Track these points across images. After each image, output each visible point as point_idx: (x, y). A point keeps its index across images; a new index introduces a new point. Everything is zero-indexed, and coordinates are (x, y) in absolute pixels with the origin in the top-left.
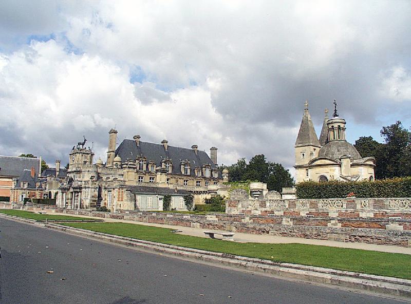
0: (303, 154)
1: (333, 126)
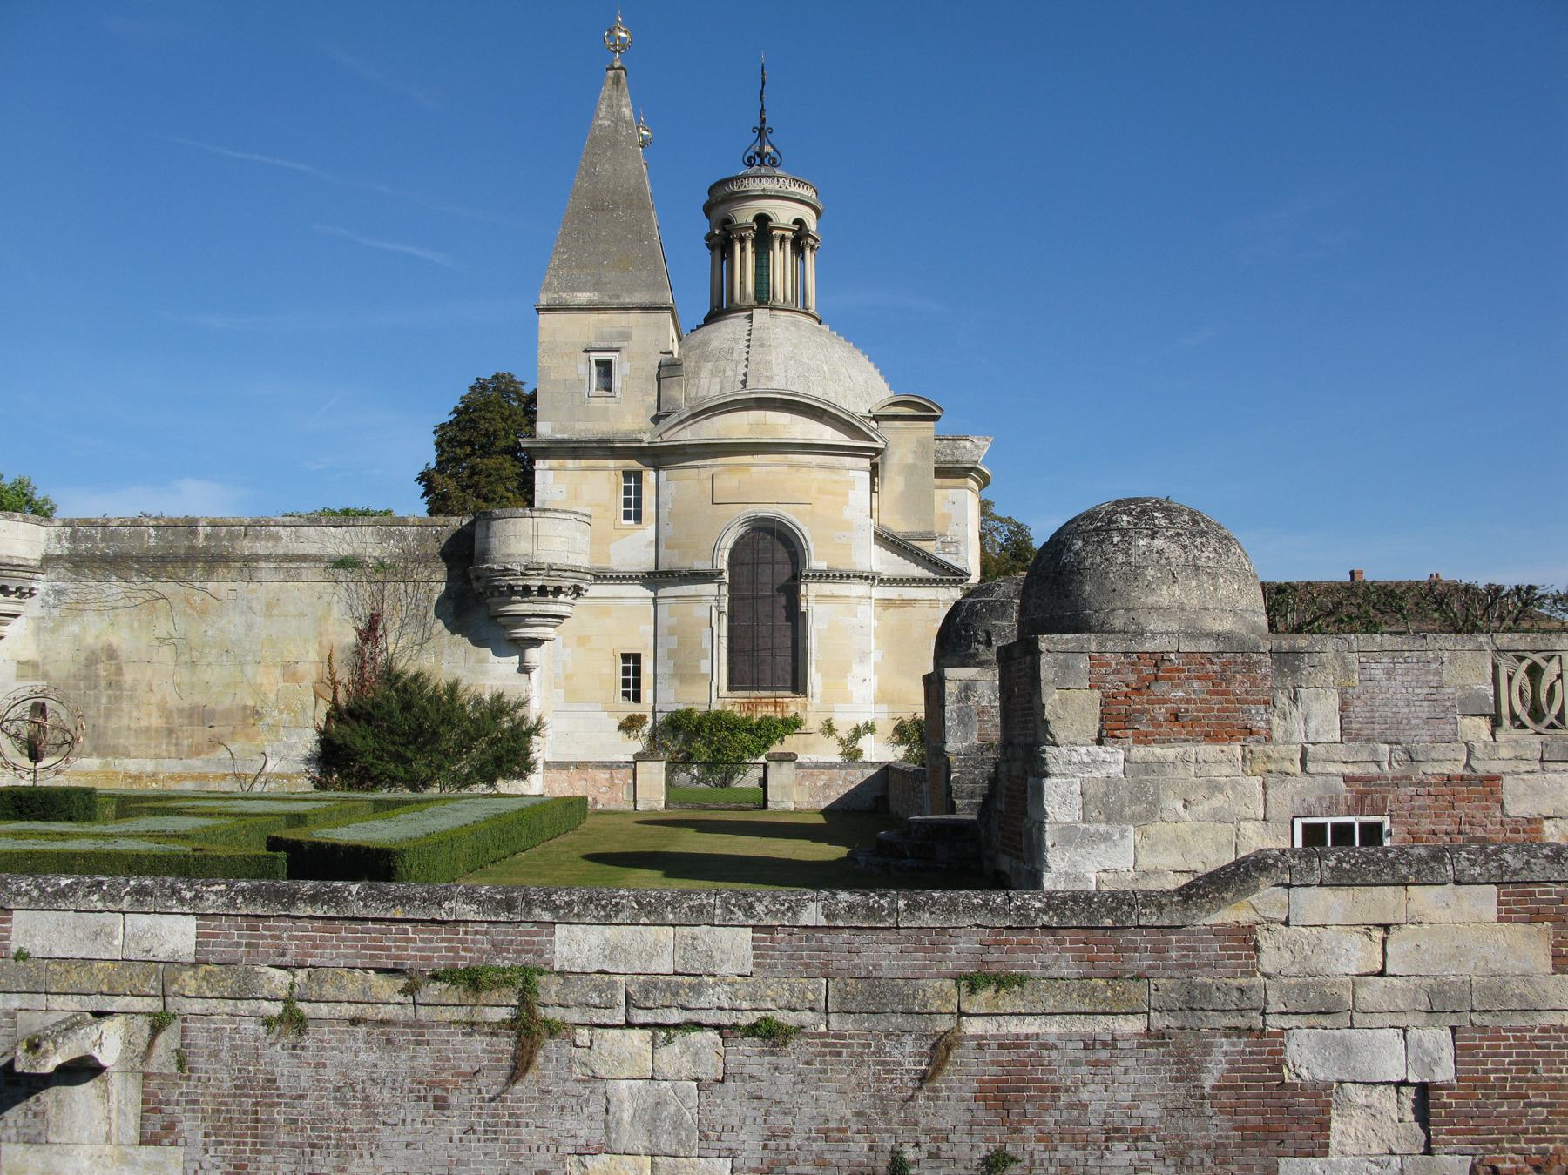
0: (605, 368)
1: (763, 219)
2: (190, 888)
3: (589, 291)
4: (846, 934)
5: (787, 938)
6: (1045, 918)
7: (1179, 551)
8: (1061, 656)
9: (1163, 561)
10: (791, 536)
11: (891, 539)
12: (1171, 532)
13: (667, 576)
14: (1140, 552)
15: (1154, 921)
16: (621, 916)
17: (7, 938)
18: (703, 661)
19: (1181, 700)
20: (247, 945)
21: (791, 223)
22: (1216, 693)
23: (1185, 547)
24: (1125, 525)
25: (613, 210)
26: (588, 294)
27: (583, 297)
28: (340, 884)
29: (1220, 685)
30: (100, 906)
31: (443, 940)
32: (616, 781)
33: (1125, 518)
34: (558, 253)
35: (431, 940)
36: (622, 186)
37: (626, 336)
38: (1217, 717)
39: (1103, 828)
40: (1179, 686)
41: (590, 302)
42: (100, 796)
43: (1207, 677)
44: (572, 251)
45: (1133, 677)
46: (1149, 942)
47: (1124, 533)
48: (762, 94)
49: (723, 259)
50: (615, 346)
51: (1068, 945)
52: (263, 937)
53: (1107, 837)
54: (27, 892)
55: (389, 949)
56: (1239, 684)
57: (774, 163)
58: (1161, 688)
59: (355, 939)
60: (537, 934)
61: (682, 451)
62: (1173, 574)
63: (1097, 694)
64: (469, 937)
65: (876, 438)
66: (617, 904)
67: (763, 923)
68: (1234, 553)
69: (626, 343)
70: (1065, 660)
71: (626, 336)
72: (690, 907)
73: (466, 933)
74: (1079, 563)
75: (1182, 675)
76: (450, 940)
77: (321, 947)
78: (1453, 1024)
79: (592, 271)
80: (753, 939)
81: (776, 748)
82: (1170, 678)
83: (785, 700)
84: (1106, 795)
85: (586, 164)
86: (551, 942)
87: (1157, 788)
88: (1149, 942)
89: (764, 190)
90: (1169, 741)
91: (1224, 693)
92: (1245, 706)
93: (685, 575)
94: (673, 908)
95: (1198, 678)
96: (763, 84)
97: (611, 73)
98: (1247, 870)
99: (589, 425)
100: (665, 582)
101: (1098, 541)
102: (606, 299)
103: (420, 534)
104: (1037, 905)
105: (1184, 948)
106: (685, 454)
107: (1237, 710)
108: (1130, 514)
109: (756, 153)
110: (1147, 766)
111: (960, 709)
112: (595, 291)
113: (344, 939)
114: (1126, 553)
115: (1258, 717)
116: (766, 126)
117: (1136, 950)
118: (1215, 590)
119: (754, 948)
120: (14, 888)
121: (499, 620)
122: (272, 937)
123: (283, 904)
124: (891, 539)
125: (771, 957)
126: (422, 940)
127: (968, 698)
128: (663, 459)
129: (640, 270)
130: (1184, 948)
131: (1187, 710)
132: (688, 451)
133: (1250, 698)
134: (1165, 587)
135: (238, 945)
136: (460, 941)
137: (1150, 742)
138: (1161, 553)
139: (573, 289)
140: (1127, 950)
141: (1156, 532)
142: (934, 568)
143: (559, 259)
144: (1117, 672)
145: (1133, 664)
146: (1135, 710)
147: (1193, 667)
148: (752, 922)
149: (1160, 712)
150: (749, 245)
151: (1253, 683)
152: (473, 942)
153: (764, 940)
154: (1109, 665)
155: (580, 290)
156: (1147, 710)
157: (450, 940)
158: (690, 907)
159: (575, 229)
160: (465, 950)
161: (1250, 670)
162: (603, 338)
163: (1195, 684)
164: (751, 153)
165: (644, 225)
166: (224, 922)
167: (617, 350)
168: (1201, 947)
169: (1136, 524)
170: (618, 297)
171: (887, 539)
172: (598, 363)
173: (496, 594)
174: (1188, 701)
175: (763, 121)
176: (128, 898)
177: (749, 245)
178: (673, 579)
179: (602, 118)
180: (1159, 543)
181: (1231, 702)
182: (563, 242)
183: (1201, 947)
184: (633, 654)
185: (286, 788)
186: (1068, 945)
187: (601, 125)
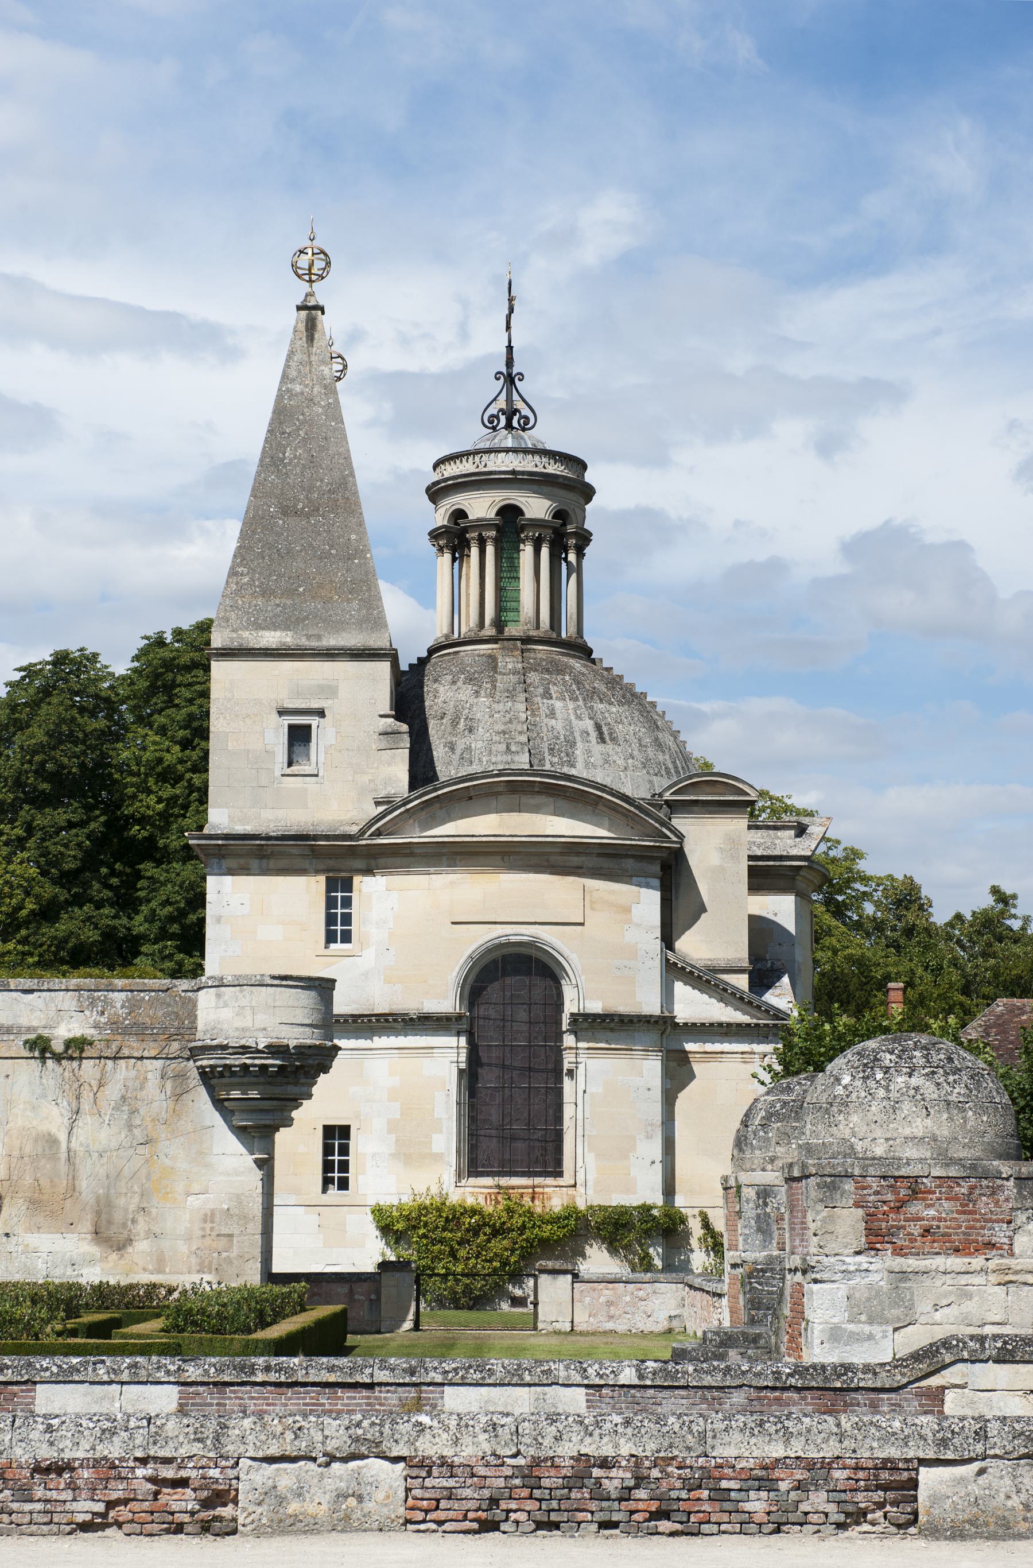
1: (510, 513)
2: (173, 1364)
4: (651, 1392)
5: (611, 1394)
6: (793, 1380)
7: (932, 1088)
8: (829, 1180)
9: (919, 1097)
10: (553, 966)
11: (689, 969)
12: (927, 1070)
13: (387, 1021)
14: (897, 1088)
15: (870, 1384)
16: (493, 1378)
17: (33, 1403)
18: (435, 1137)
19: (933, 1219)
20: (217, 1404)
22: (964, 1213)
23: (938, 1084)
24: (887, 1063)
25: (308, 516)
26: (278, 633)
27: (270, 638)
28: (285, 1358)
29: (967, 1205)
30: (106, 1378)
31: (362, 1398)
32: (357, 1297)
33: (888, 1056)
35: (355, 1398)
36: (322, 481)
37: (330, 690)
38: (965, 1234)
39: (867, 1329)
40: (932, 1205)
43: (955, 1198)
44: (254, 571)
45: (889, 1197)
46: (868, 1399)
47: (886, 1070)
48: (508, 327)
49: (454, 560)
50: (315, 705)
51: (809, 1400)
52: (230, 1398)
53: (870, 1337)
54: (47, 1369)
55: (323, 1405)
56: (984, 1205)
57: (527, 423)
58: (915, 1208)
59: (298, 1399)
60: (432, 1392)
61: (408, 851)
62: (927, 1108)
63: (860, 1212)
64: (382, 1395)
65: (668, 833)
66: (489, 1370)
67: (591, 1382)
68: (986, 1088)
69: (330, 702)
70: (832, 1182)
71: (330, 690)
72: (542, 1372)
73: (380, 1392)
74: (848, 1096)
75: (934, 1196)
76: (368, 1398)
77: (273, 1404)
79: (283, 601)
80: (587, 1394)
82: (924, 1199)
83: (547, 1190)
84: (869, 1299)
86: (442, 1398)
87: (912, 1294)
88: (868, 1399)
90: (923, 1254)
91: (970, 1213)
92: (989, 1225)
93: (411, 1019)
94: (530, 1371)
95: (946, 1199)
96: (511, 310)
98: (937, 1347)
99: (281, 814)
100: (384, 1028)
101: (863, 1077)
102: (304, 642)
103: (128, 1000)
104: (788, 1371)
105: (892, 1405)
106: (411, 854)
107: (983, 1228)
108: (892, 1053)
109: (501, 410)
110: (903, 1275)
111: (758, 1216)
112: (287, 628)
113: (290, 1399)
114: (887, 1089)
115: (1000, 1234)
116: (515, 371)
117: (858, 1405)
118: (965, 1122)
119: (588, 1401)
120: (38, 1366)
121: (226, 1104)
122: (237, 1398)
123: (245, 1373)
124: (689, 969)
125: (600, 1407)
126: (348, 1398)
127: (766, 1204)
128: (382, 861)
129: (349, 601)
130: (892, 1405)
131: (938, 1227)
132: (416, 851)
133: (994, 1217)
134: (919, 1120)
135: (211, 1405)
136: (376, 1398)
137: (906, 1254)
138: (917, 1089)
139: (259, 627)
140: (852, 1405)
141: (914, 1071)
142: (754, 1012)
143: (237, 583)
144: (876, 1193)
145: (891, 1186)
146: (893, 1227)
147: (944, 1190)
148: (586, 1382)
149: (916, 1230)
150: (490, 550)
151: (997, 1203)
152: (385, 1398)
153: (594, 1395)
154: (870, 1187)
156: (904, 1227)
157: (368, 1398)
158: (800, 1146)
160: (381, 1405)
161: (993, 1193)
162: (298, 694)
163: (946, 1204)
164: (493, 410)
165: (353, 537)
166: (201, 1389)
167: (321, 713)
168: (905, 1404)
169: (896, 1063)
170: (319, 637)
171: (683, 968)
172: (291, 727)
173: (227, 1074)
174: (940, 1220)
175: (510, 362)
176: (127, 1371)
177: (490, 550)
178: (395, 1025)
180: (914, 1081)
181: (978, 1221)
183: (905, 1404)
184: (340, 1126)
186: (809, 1400)
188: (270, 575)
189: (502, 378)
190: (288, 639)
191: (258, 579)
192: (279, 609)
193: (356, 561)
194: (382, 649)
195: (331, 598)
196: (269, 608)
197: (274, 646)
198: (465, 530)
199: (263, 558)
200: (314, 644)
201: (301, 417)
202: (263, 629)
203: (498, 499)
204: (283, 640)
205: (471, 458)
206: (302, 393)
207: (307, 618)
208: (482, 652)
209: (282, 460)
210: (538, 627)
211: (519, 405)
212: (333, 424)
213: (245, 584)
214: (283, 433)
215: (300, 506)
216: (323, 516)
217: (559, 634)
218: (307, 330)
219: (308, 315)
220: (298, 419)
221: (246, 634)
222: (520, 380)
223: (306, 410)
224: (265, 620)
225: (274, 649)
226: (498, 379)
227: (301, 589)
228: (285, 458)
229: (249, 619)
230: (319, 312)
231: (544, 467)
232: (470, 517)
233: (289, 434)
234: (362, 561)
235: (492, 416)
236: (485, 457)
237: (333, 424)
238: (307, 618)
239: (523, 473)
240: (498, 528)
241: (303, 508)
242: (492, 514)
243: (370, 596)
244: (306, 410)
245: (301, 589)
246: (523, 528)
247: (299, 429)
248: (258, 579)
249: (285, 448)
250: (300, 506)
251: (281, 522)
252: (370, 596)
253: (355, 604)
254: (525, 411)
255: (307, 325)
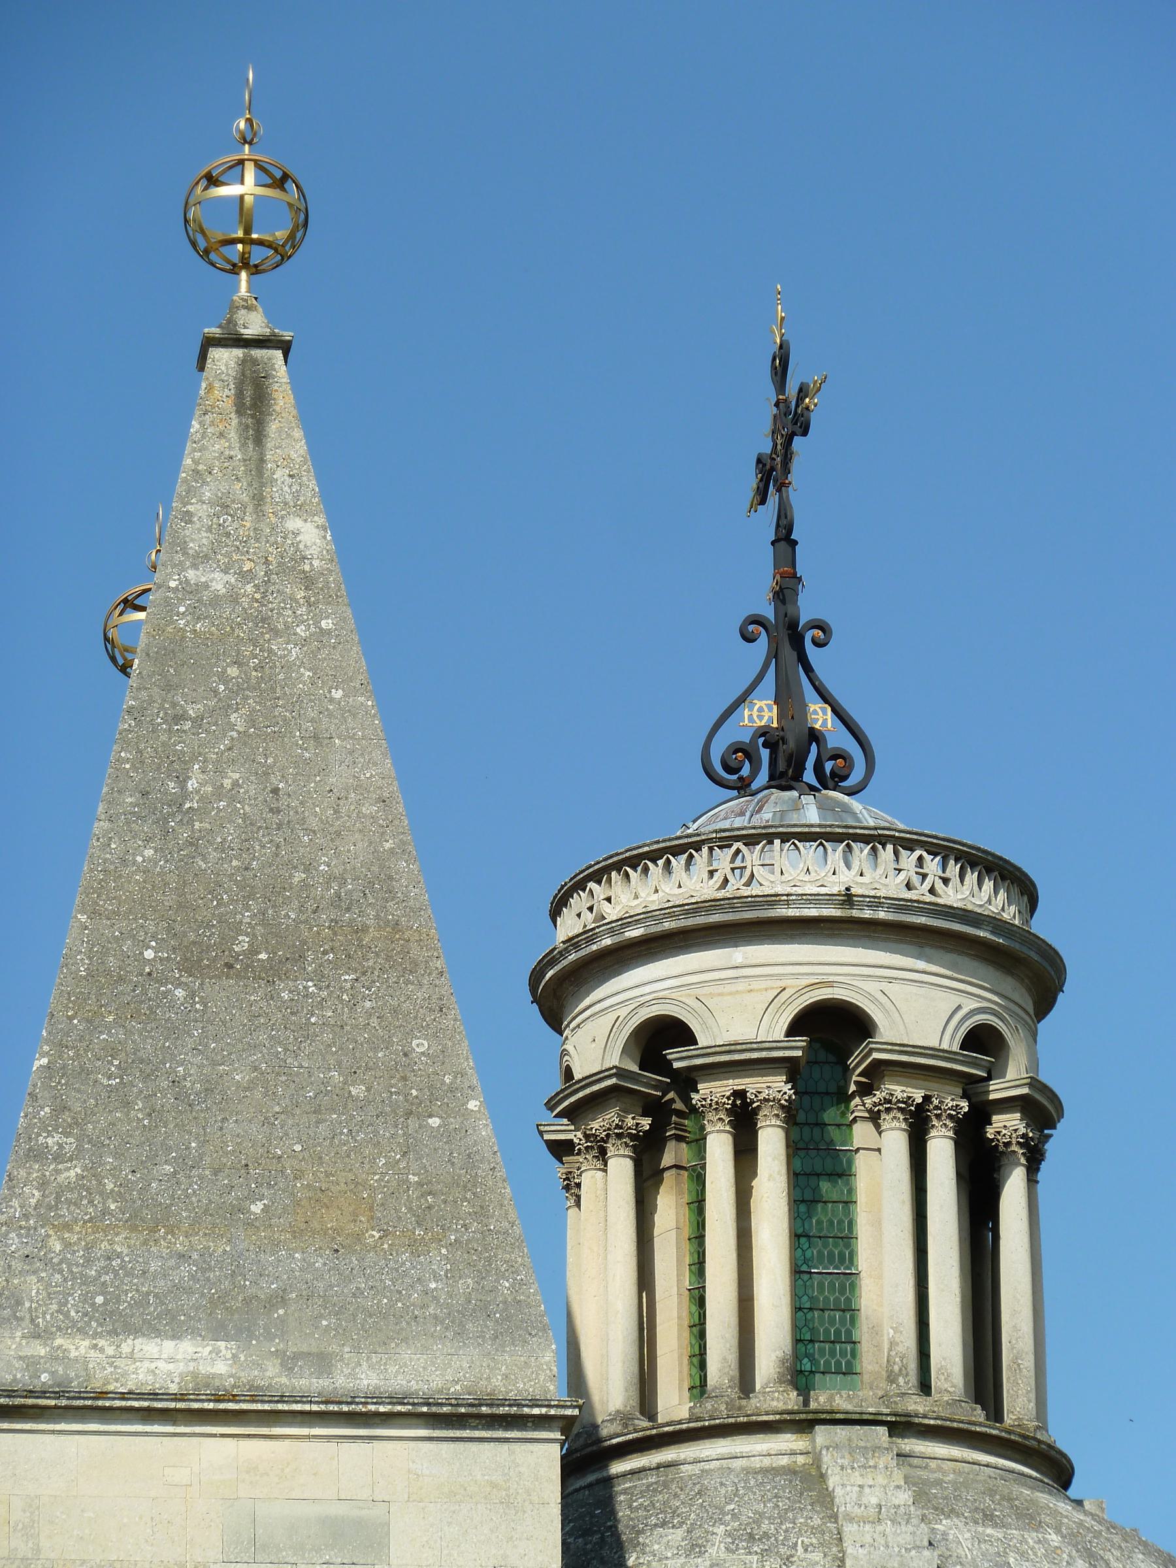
3: (194, 1333)
21: (951, 1042)
25: (273, 973)
26: (186, 1347)
34: (37, 1154)
41: (202, 1385)
42: (848, 1183)
78: (605, 896)
79: (199, 1242)
81: (773, 603)
85: (139, 763)
89: (848, 898)
97: (224, 359)
102: (272, 1375)
112: (218, 1332)
129: (416, 1247)
143: (43, 1185)
155: (151, 1330)
159: (112, 1051)
165: (420, 1045)
170: (323, 1362)
179: (201, 559)
182: (61, 1108)
185: (935, 1053)
187: (189, 590)
188: (153, 1160)
189: (763, 638)
190: (221, 1368)
191: (114, 1172)
192: (185, 1269)
193: (435, 1122)
194: (535, 1403)
195: (359, 1237)
196: (154, 1266)
197: (173, 1388)
198: (687, 1081)
199: (127, 1105)
200: (308, 1382)
201: (233, 671)
202: (136, 1332)
203: (794, 984)
204: (205, 1369)
205: (701, 857)
206: (233, 598)
207: (280, 1299)
208: (757, 1463)
209: (177, 803)
210: (925, 1387)
211: (820, 717)
212: (338, 694)
213: (69, 1188)
214: (179, 718)
215: (243, 943)
216: (319, 977)
217: (996, 1412)
218: (240, 410)
219: (243, 363)
220: (224, 678)
221: (78, 1347)
222: (818, 644)
223: (247, 650)
224: (142, 1304)
225: (176, 1398)
226: (748, 638)
227: (257, 1208)
228: (185, 795)
229: (87, 1298)
230: (279, 354)
231: (932, 891)
232: (703, 1041)
233: (198, 721)
234: (454, 1123)
235: (737, 748)
236: (752, 857)
237: (338, 694)
238: (280, 1299)
239: (876, 902)
240: (791, 1069)
241: (253, 951)
242: (775, 1028)
243: (486, 1233)
244: (247, 650)
245: (257, 1208)
246: (877, 1072)
247: (227, 709)
248: (114, 1172)
249: (187, 765)
250: (243, 943)
251: (180, 993)
252: (486, 1233)
253: (438, 1258)
254: (838, 737)
255: (240, 395)
